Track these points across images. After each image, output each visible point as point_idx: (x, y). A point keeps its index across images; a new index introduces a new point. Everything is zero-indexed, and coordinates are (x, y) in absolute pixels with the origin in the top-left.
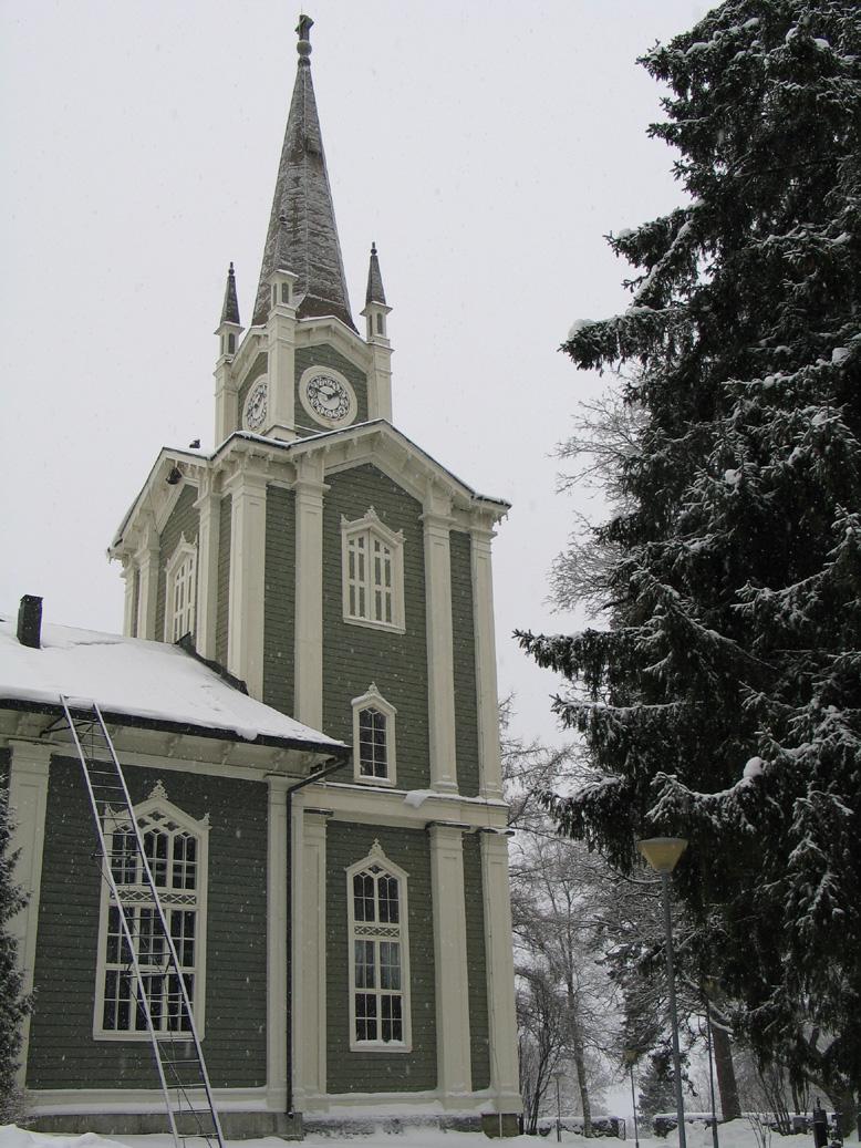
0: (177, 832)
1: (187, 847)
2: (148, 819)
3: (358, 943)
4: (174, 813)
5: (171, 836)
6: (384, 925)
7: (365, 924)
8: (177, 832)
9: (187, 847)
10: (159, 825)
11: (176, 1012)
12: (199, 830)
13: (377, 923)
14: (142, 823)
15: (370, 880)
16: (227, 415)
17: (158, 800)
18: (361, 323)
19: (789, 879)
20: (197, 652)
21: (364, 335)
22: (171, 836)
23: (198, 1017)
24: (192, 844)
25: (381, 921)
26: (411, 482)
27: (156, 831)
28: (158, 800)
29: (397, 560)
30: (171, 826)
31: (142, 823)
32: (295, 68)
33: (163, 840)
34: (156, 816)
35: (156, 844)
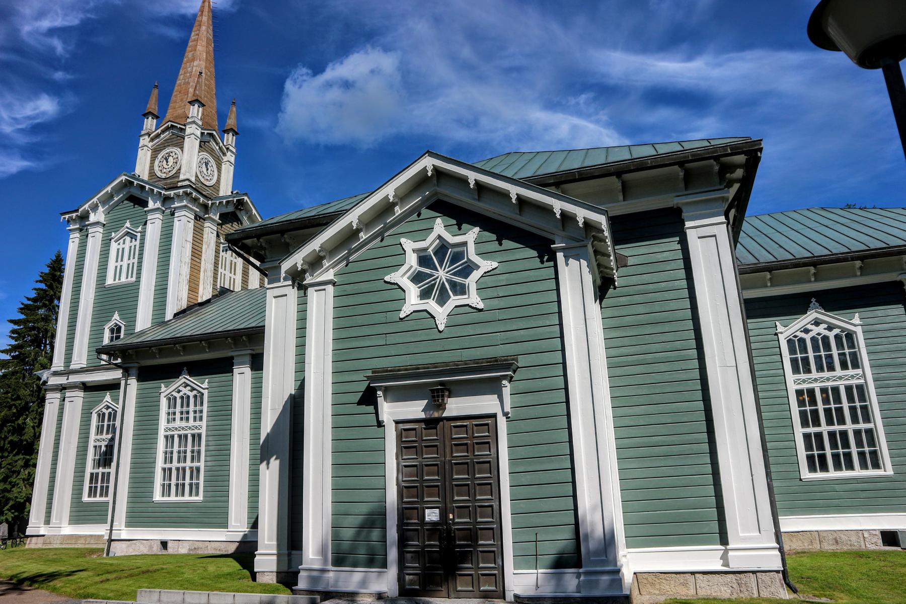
2: (809, 327)
3: (799, 393)
5: (831, 335)
6: (821, 375)
7: (196, 431)
10: (821, 329)
11: (871, 453)
13: (815, 374)
14: (807, 331)
15: (802, 341)
19: (380, 388)
20: (231, 559)
22: (831, 335)
23: (164, 402)
24: (850, 336)
25: (818, 371)
26: (202, 199)
27: (819, 334)
31: (179, 391)
33: (825, 339)
34: (817, 323)
35: (185, 400)
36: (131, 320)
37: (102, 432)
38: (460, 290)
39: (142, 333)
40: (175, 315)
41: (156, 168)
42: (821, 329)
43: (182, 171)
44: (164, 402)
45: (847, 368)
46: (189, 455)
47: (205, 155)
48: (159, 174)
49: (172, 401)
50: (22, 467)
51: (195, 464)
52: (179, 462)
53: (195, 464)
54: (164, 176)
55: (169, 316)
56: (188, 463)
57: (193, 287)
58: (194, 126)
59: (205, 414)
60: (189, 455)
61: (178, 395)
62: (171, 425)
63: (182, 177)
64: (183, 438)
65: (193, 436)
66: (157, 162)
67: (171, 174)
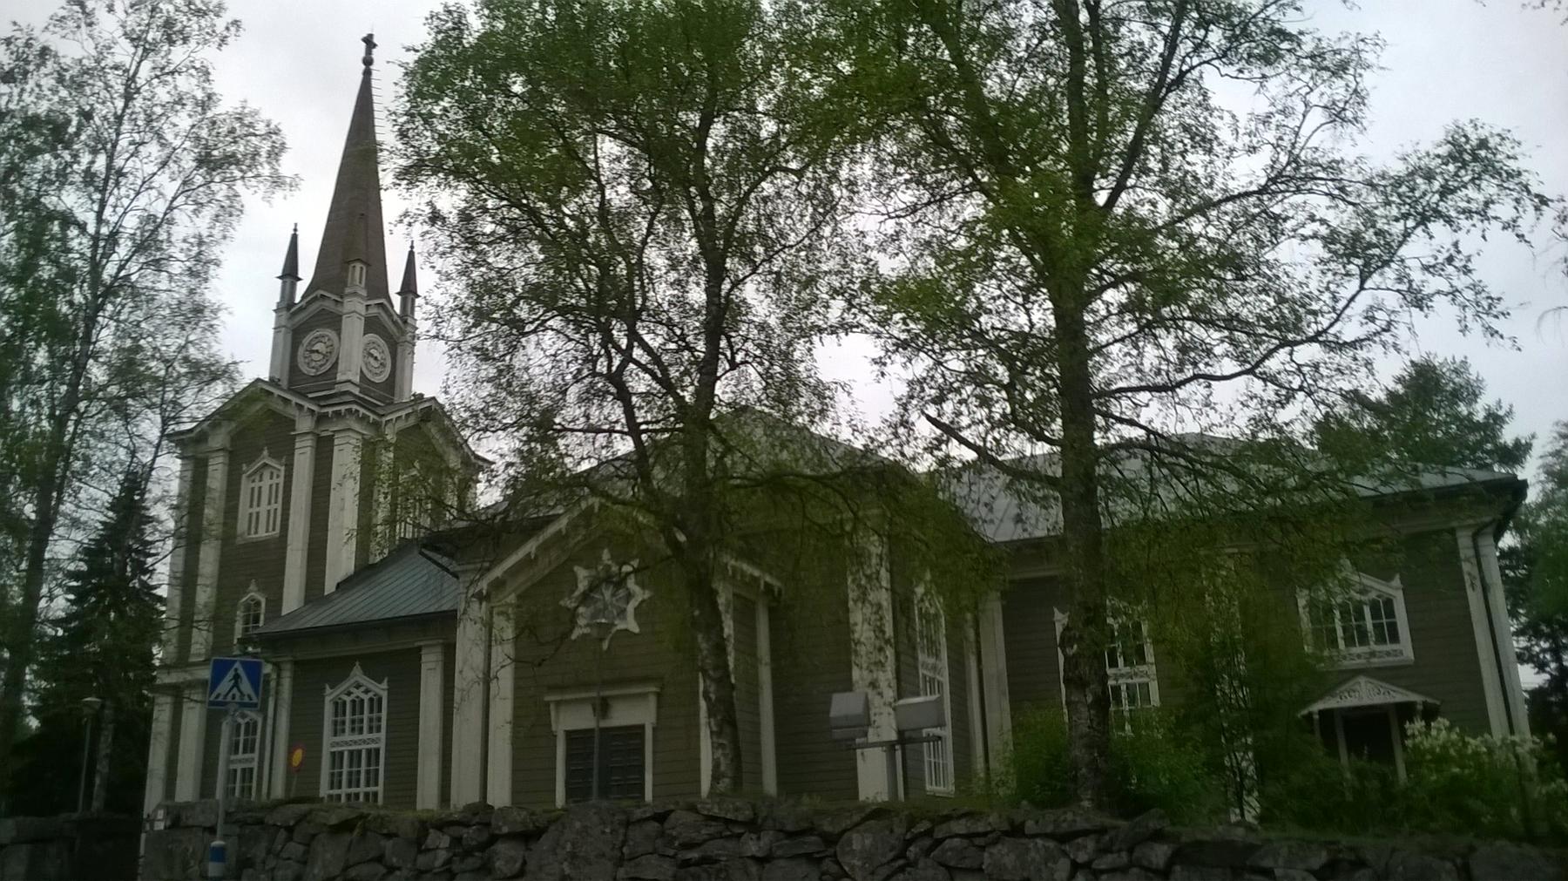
0: (370, 695)
1: (1383, 608)
4: (367, 682)
7: (373, 746)
8: (370, 695)
9: (376, 703)
12: (382, 689)
16: (403, 370)
17: (357, 674)
18: (397, 301)
21: (397, 308)
23: (328, 709)
24: (1389, 603)
28: (357, 674)
29: (244, 510)
30: (1363, 591)
31: (349, 694)
32: (360, 77)
34: (358, 686)
35: (357, 705)
36: (276, 602)
37: (236, 752)
38: (629, 596)
39: (293, 615)
40: (338, 585)
41: (300, 360)
42: (358, 693)
43: (341, 367)
44: (328, 709)
45: (1384, 642)
46: (345, 777)
47: (371, 337)
48: (305, 369)
49: (339, 707)
50: (670, 252)
51: (372, 789)
52: (350, 786)
53: (372, 789)
54: (312, 372)
55: (330, 587)
56: (345, 790)
57: (363, 549)
58: (355, 299)
59: (384, 724)
60: (345, 777)
61: (348, 699)
62: (337, 739)
63: (340, 378)
64: (355, 756)
65: (369, 751)
66: (301, 351)
67: (323, 370)
